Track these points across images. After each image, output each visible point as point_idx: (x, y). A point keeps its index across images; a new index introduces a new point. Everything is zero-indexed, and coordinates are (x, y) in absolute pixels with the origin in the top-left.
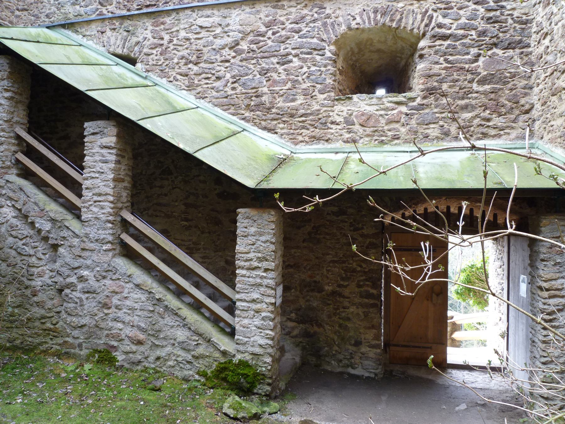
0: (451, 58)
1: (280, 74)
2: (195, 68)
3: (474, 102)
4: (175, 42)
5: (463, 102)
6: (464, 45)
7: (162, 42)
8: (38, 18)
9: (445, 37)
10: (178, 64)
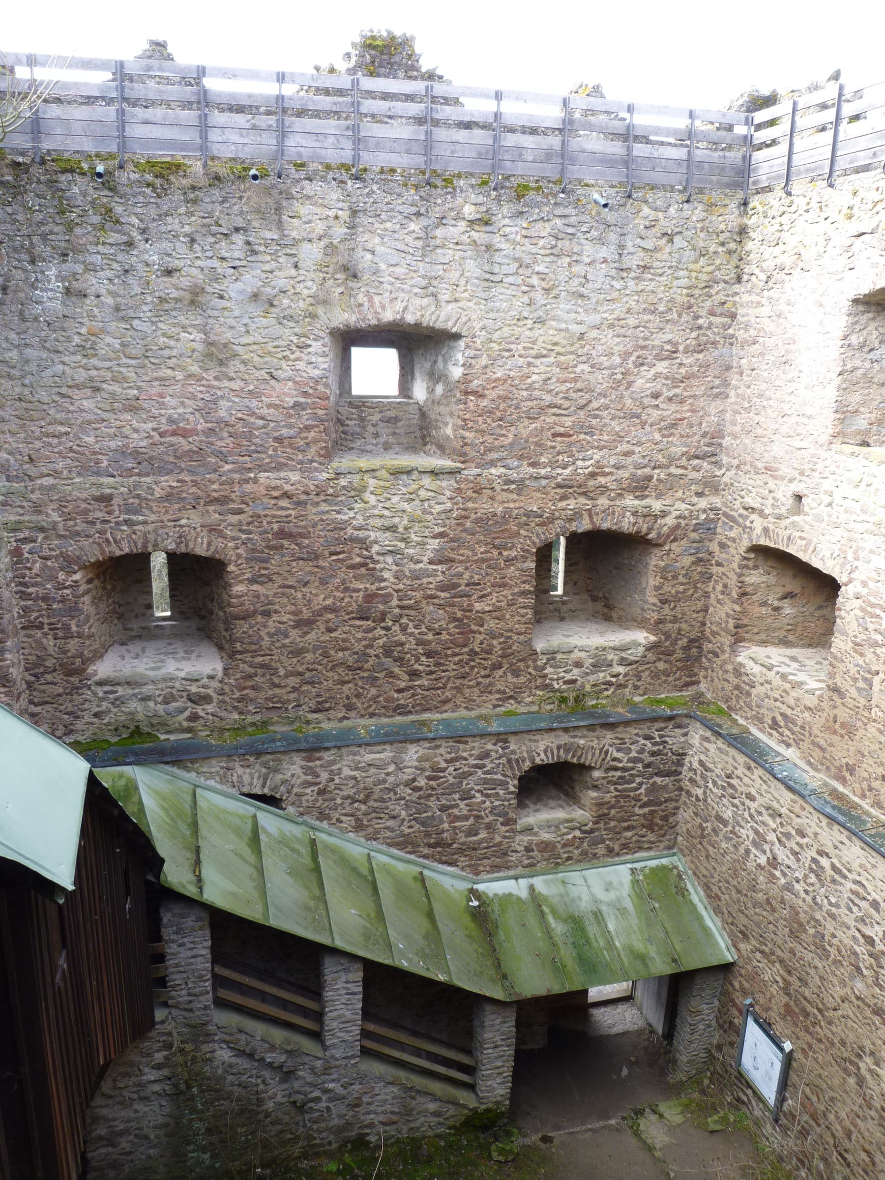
0: (620, 787)
1: (463, 808)
2: (363, 807)
3: (634, 824)
4: (337, 781)
5: (625, 824)
6: (631, 775)
7: (318, 780)
8: (78, 717)
9: (616, 769)
10: (342, 804)
